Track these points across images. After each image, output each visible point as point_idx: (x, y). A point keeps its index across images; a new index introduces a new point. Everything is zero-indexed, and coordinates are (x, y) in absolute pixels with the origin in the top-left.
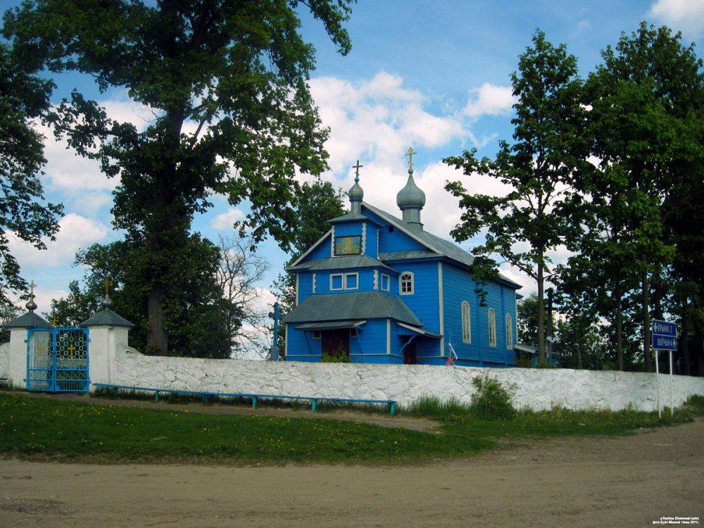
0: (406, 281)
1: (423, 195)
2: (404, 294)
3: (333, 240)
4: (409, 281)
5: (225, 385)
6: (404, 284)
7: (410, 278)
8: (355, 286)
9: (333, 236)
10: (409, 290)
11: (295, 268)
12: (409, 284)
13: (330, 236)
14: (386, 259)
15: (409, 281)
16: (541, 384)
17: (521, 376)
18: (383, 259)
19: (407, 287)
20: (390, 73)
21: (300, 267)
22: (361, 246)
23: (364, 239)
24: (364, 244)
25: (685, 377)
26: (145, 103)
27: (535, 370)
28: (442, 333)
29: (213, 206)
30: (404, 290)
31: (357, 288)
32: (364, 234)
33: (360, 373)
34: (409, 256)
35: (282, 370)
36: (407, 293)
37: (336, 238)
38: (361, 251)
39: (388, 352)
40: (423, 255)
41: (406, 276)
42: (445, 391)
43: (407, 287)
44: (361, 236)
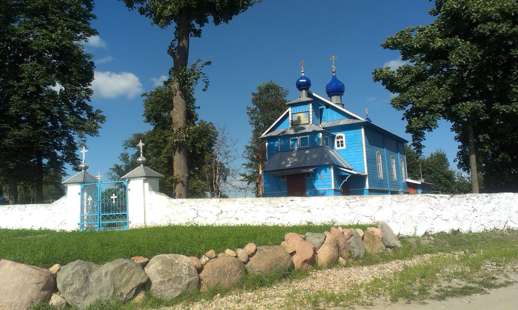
0: (340, 140)
1: (343, 86)
2: (339, 148)
3: (290, 116)
4: (342, 140)
5: (237, 219)
6: (338, 142)
7: (342, 137)
8: (308, 145)
9: (290, 113)
10: (342, 145)
11: (266, 136)
12: (342, 142)
13: (288, 113)
14: (326, 127)
15: (342, 140)
16: (492, 205)
17: (476, 200)
18: (324, 126)
19: (340, 144)
20: (117, 73)
21: (269, 135)
22: (309, 118)
23: (311, 113)
24: (311, 117)
25: (316, 197)
26: (231, 19)
27: (486, 194)
28: (366, 173)
29: (252, 93)
30: (338, 146)
31: (308, 146)
32: (311, 110)
33: (348, 204)
34: (341, 123)
35: (282, 204)
36: (340, 148)
37: (292, 114)
38: (309, 121)
39: (333, 188)
40: (351, 121)
41: (340, 136)
42: (421, 215)
43: (340, 144)
44: (309, 112)
